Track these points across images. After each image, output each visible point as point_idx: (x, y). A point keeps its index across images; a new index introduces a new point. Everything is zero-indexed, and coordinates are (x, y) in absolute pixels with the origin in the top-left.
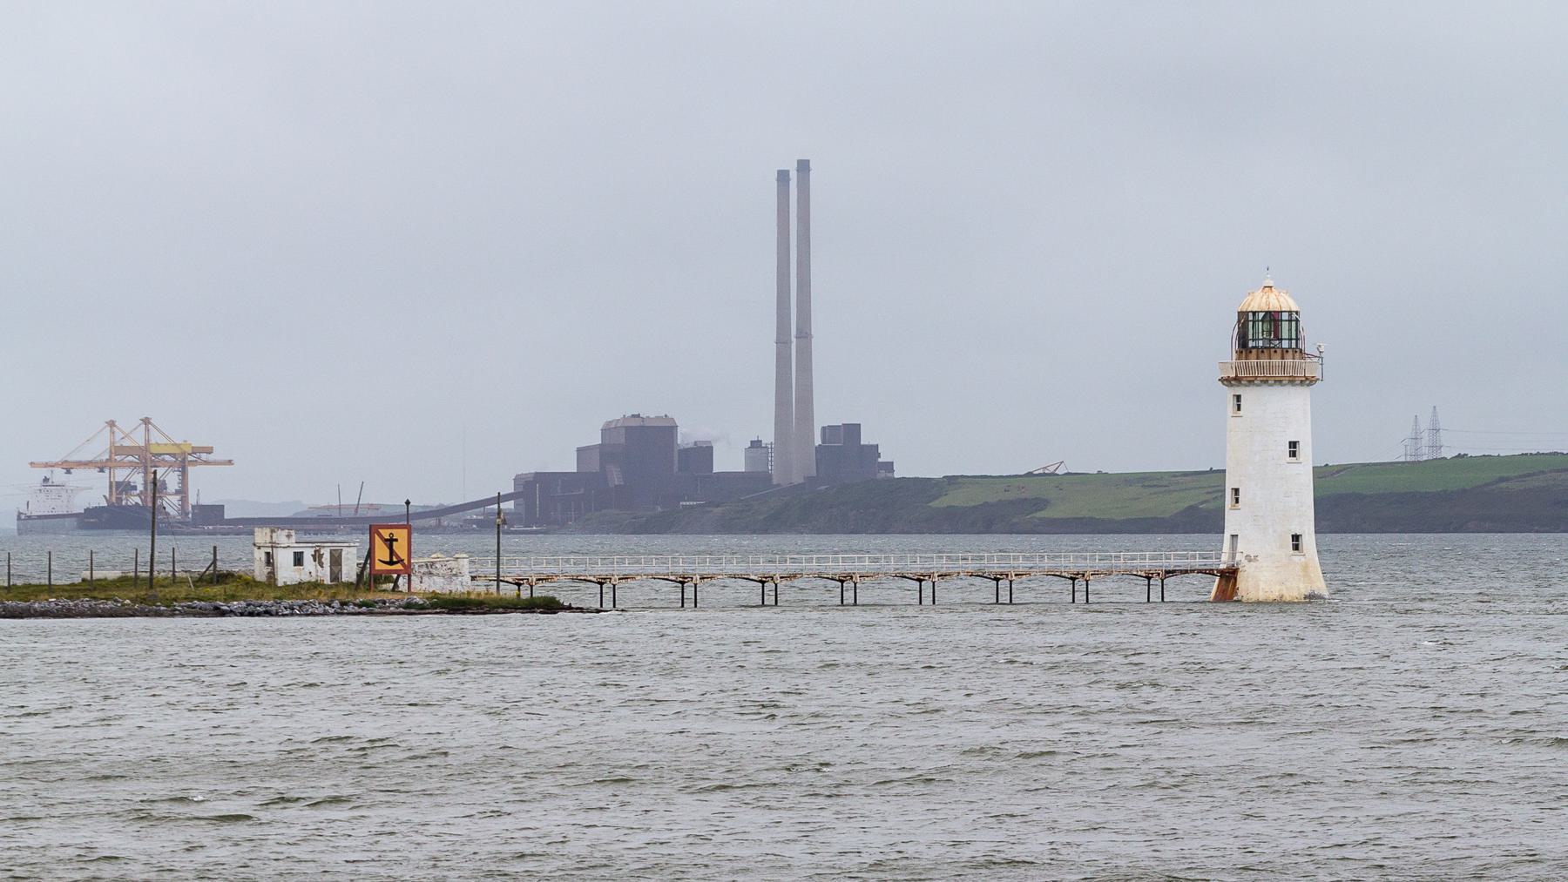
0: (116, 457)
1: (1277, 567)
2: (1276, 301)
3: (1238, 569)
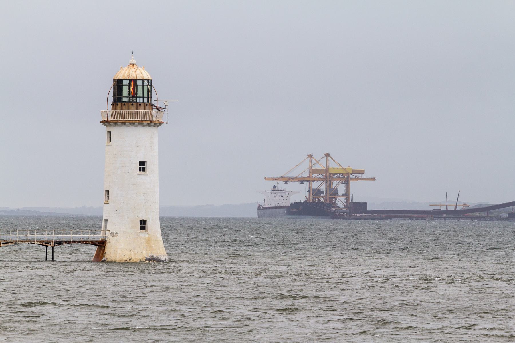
0: (313, 175)
1: (129, 240)
2: (134, 73)
3: (106, 241)
